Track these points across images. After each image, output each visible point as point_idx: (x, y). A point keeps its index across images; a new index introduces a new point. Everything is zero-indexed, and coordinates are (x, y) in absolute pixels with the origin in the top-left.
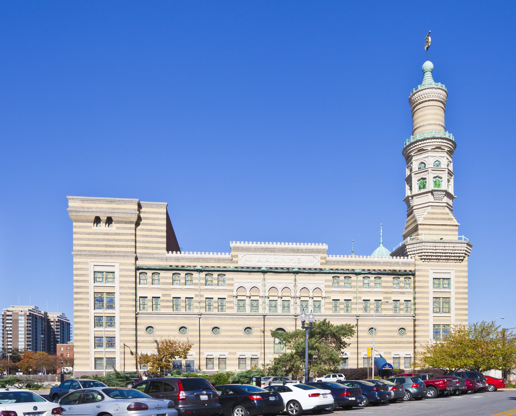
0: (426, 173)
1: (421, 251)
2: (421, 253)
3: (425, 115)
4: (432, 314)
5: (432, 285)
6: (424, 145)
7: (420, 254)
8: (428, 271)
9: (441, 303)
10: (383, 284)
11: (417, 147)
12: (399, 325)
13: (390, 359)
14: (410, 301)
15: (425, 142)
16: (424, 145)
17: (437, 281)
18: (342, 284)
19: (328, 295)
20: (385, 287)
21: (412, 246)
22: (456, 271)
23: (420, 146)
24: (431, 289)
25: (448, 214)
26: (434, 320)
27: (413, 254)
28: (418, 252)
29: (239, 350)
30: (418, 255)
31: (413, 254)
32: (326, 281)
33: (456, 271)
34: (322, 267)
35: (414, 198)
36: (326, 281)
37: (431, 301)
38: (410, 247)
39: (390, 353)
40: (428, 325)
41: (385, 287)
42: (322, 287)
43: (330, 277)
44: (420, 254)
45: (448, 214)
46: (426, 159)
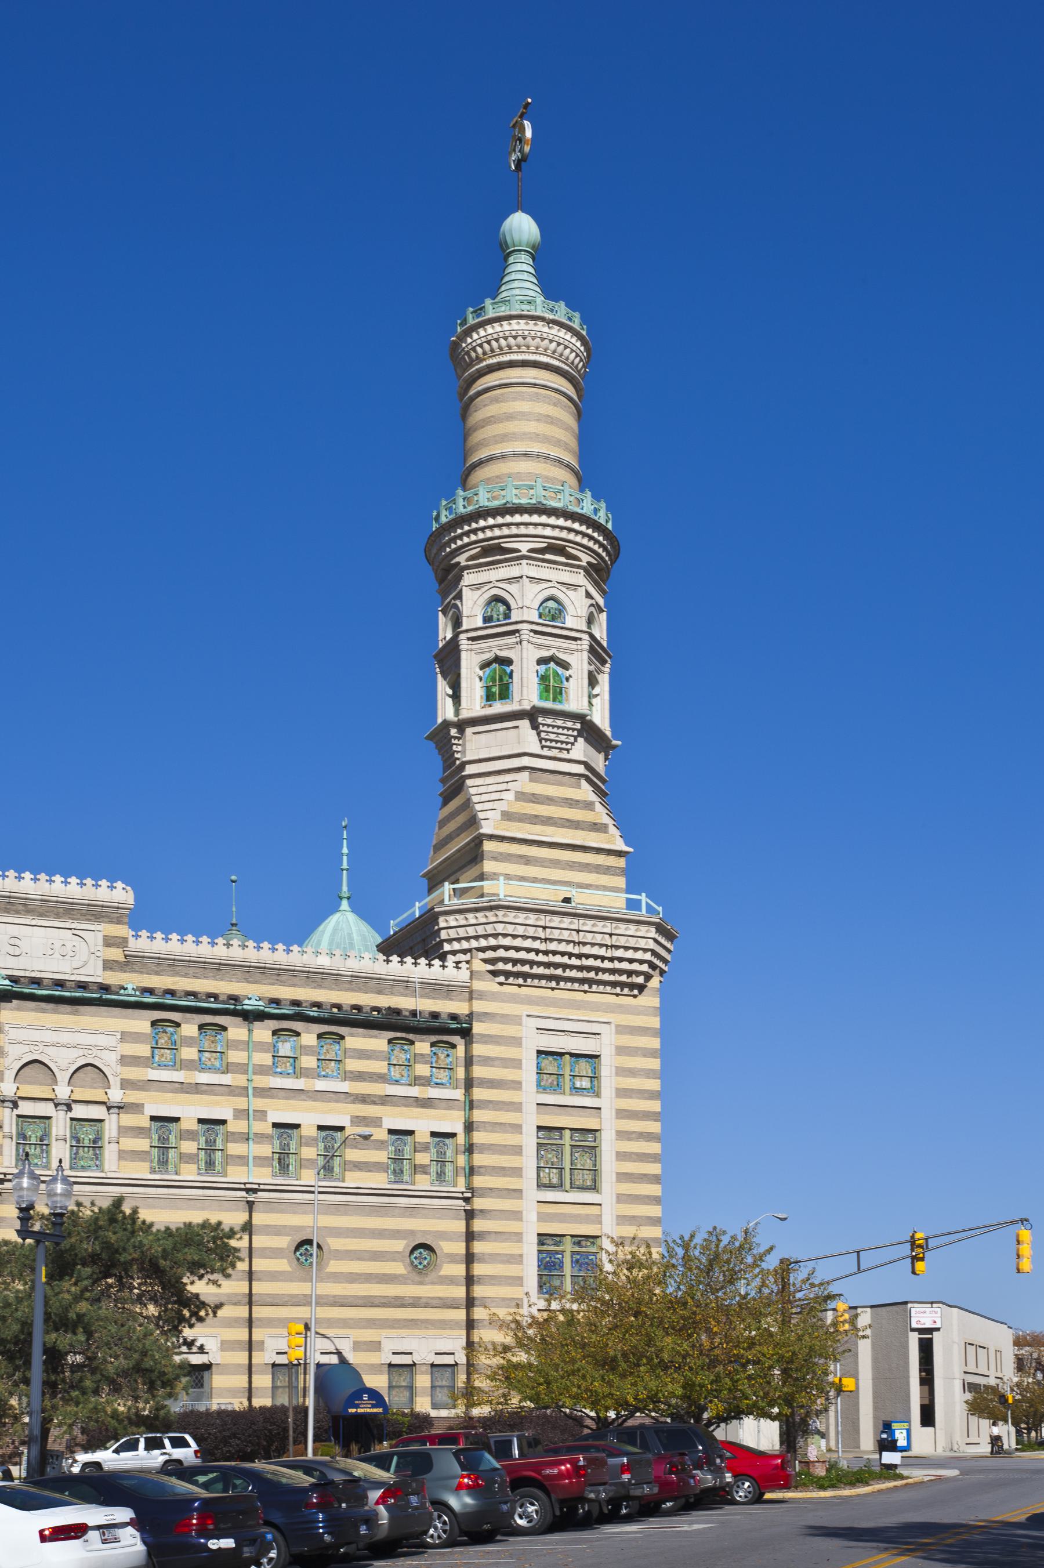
0: (511, 640)
1: (492, 942)
2: (494, 948)
3: (509, 417)
4: (532, 1194)
5: (534, 1077)
6: (506, 531)
7: (490, 954)
8: (516, 1020)
9: (567, 1150)
10: (353, 1065)
11: (481, 535)
12: (412, 1233)
13: (375, 1369)
14: (453, 1135)
15: (508, 519)
16: (506, 531)
17: (550, 1065)
18: (189, 1053)
19: (133, 1096)
20: (360, 1076)
21: (461, 919)
22: (621, 1029)
23: (489, 534)
24: (529, 1095)
25: (589, 806)
26: (542, 1217)
27: (464, 952)
28: (483, 943)
29: (393, 1332)
30: (481, 955)
31: (464, 952)
32: (126, 1037)
33: (621, 1029)
34: (112, 978)
35: (469, 731)
36: (126, 1037)
37: (529, 1140)
38: (452, 921)
39: (376, 1346)
40: (518, 1237)
41: (360, 1076)
42: (109, 1062)
43: (140, 1023)
44: (490, 954)
45: (589, 806)
46: (513, 588)
